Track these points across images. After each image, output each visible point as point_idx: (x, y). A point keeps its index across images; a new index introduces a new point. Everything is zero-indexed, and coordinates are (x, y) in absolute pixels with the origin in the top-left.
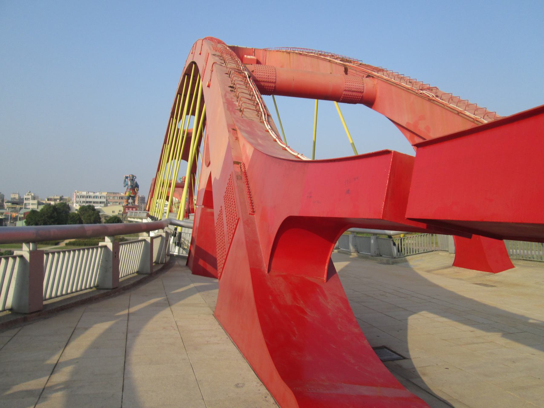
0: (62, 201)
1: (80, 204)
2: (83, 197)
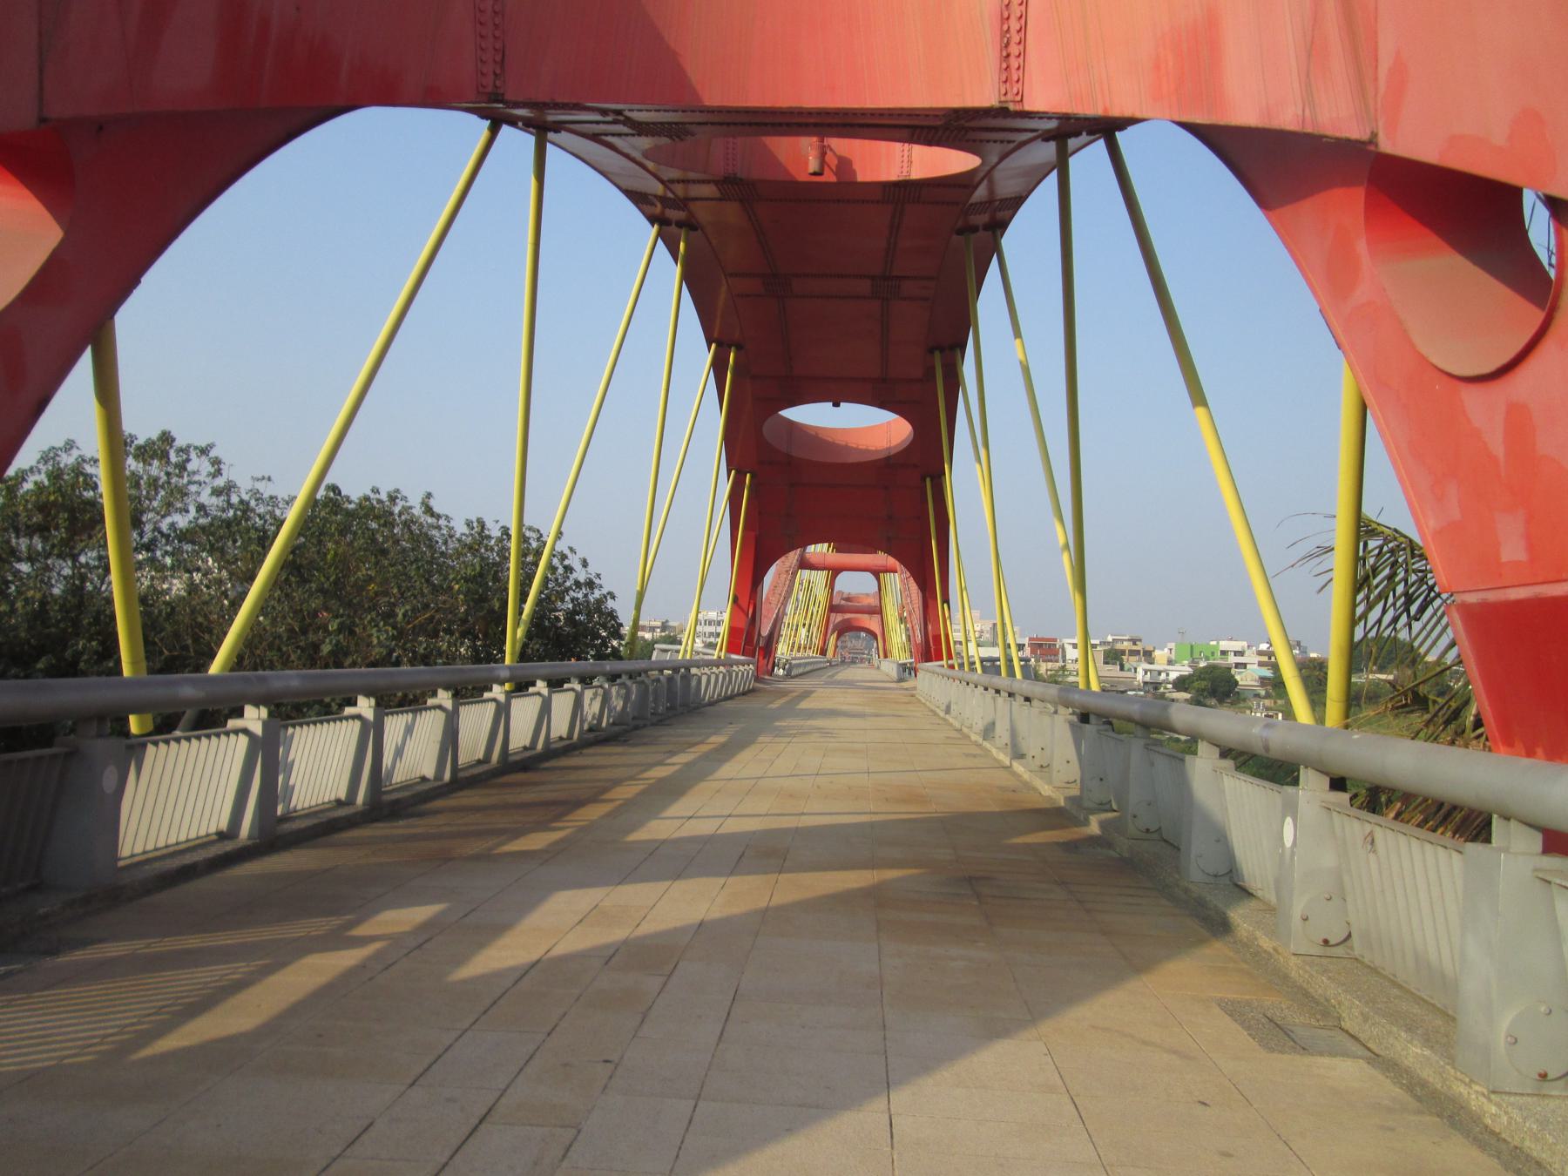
0: (667, 633)
1: (705, 639)
2: (710, 624)
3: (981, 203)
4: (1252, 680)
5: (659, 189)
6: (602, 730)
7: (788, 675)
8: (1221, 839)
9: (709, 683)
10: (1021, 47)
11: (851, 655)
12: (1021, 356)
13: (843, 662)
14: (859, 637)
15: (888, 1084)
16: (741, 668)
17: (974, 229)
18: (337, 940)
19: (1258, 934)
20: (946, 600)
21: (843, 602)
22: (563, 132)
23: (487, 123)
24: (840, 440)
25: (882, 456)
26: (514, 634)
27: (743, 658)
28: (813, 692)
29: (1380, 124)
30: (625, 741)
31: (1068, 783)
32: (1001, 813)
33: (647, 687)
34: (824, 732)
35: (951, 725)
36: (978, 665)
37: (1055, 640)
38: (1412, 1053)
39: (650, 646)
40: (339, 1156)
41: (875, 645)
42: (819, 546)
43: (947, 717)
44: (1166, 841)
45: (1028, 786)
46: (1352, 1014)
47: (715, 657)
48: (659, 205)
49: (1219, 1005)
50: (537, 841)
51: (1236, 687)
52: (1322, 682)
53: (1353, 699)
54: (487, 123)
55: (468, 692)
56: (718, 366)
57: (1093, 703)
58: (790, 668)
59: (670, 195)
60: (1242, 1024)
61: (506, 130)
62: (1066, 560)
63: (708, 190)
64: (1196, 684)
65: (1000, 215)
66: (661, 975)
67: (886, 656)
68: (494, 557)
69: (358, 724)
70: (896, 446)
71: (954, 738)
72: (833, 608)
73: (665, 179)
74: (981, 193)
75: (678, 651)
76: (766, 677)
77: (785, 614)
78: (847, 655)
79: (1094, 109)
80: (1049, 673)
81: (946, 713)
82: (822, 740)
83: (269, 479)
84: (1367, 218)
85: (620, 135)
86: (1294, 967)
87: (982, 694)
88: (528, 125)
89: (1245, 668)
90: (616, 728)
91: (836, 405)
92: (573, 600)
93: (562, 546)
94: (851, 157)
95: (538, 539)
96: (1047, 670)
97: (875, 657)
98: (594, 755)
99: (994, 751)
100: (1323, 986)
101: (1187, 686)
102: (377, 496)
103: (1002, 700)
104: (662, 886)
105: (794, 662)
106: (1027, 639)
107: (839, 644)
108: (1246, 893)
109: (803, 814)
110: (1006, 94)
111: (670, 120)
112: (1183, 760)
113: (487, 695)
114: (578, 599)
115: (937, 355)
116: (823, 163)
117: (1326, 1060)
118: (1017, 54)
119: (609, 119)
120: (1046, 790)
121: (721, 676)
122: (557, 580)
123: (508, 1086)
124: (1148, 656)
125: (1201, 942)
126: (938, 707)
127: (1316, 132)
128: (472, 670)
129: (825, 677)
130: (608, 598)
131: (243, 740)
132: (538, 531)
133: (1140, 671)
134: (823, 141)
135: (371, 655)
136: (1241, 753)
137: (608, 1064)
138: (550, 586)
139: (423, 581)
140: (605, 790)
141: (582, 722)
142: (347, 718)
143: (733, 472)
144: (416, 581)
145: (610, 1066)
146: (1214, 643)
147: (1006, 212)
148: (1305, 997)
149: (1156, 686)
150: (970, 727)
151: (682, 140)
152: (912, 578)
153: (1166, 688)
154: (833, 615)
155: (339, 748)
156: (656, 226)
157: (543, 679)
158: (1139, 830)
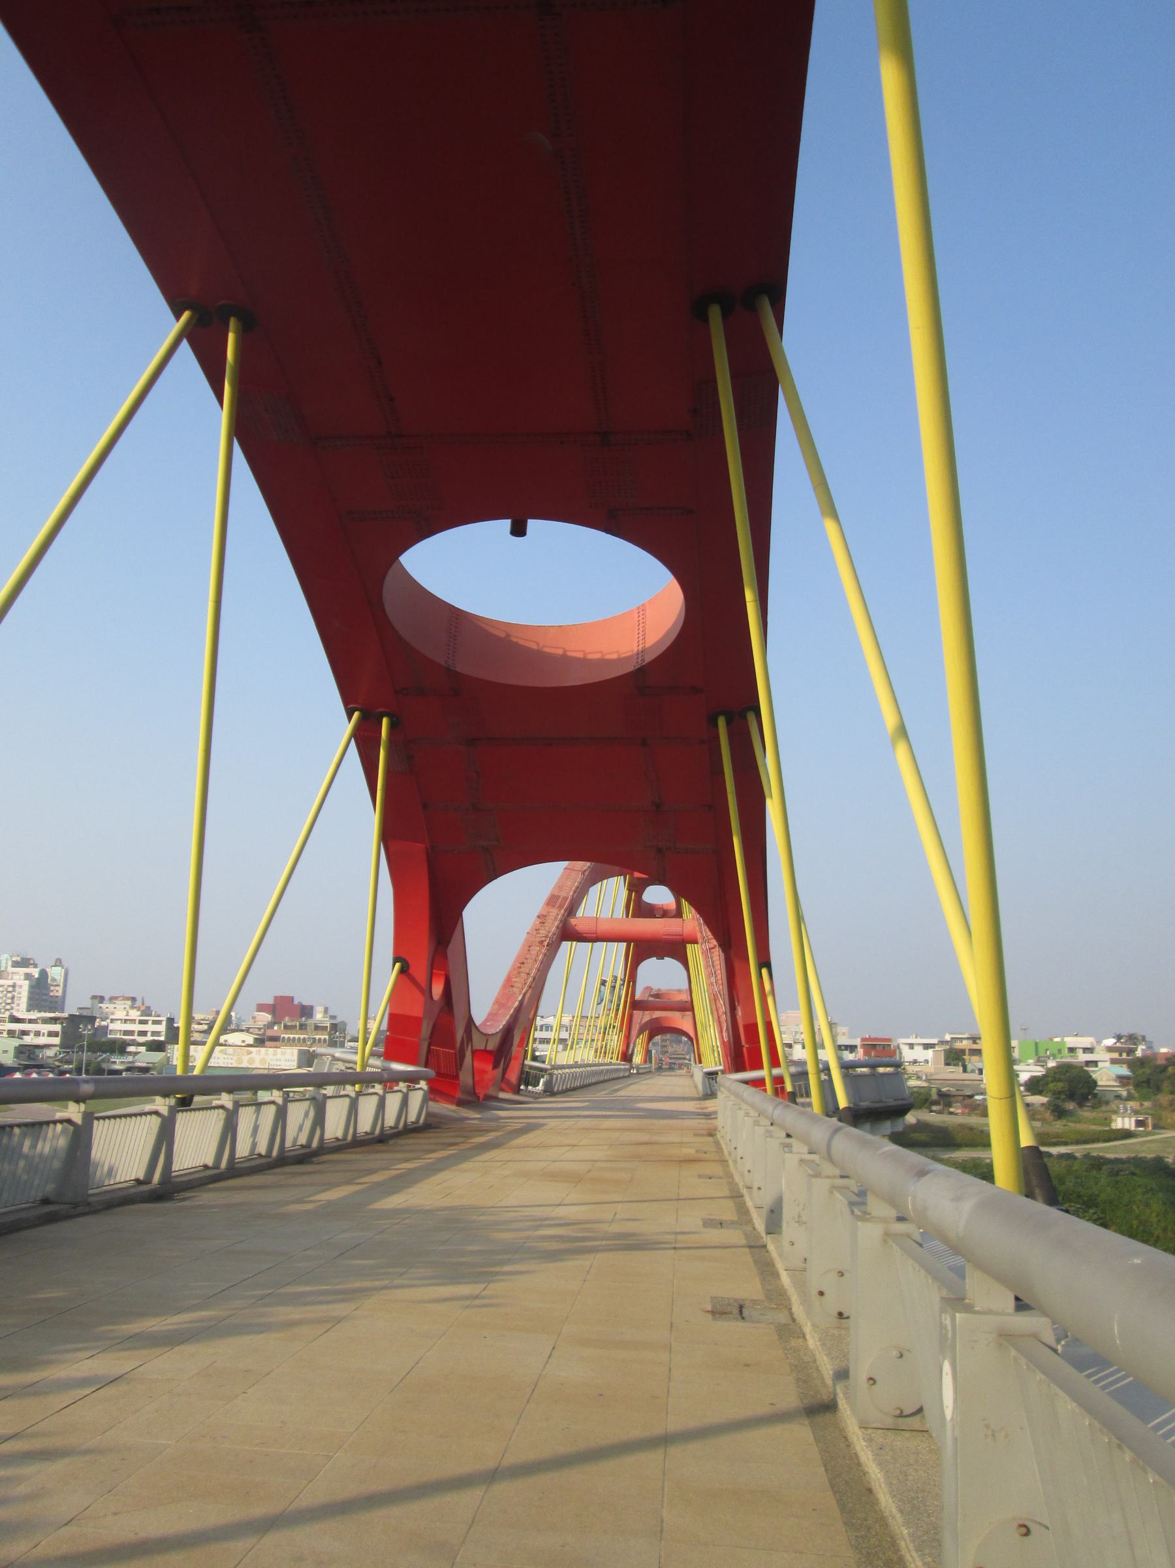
4: (1107, 1080)
14: (680, 1042)
20: (765, 962)
24: (553, 647)
25: (630, 668)
89: (1097, 1066)
101: (1041, 1088)
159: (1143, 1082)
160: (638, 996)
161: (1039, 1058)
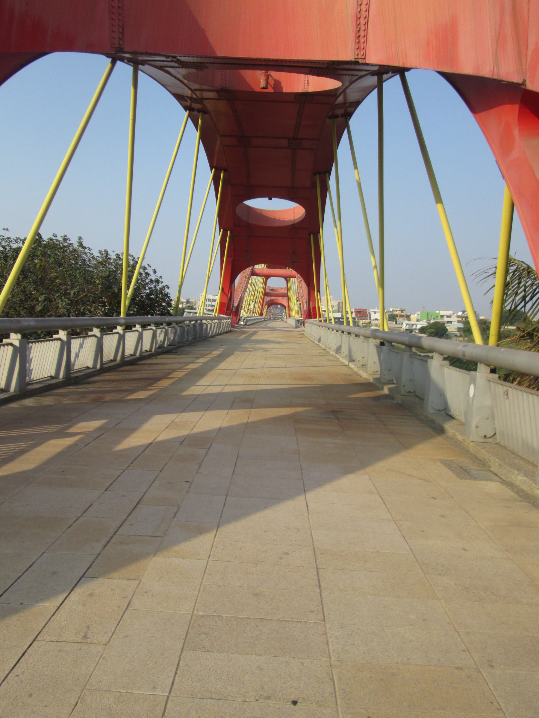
1: (206, 308)
2: (209, 301)
3: (341, 104)
4: (454, 329)
5: (188, 93)
6: (165, 348)
7: (246, 325)
8: (442, 395)
9: (211, 327)
10: (366, 32)
11: (273, 316)
12: (357, 178)
13: (270, 319)
14: (277, 308)
15: (305, 491)
16: (225, 321)
17: (337, 116)
18: (62, 434)
19: (457, 434)
20: (319, 291)
21: (270, 292)
22: (146, 65)
23: (110, 60)
25: (291, 223)
26: (124, 303)
27: (226, 316)
28: (258, 332)
29: (528, 76)
30: (175, 353)
31: (374, 372)
32: (345, 385)
33: (184, 329)
34: (264, 350)
35: (321, 347)
36: (333, 321)
37: (366, 310)
38: (519, 479)
39: (183, 310)
40: (81, 516)
41: (285, 311)
42: (260, 265)
43: (319, 344)
44: (417, 396)
45: (356, 373)
46: (495, 464)
47: (213, 316)
48: (189, 101)
49: (440, 462)
50: (143, 395)
51: (446, 332)
52: (488, 328)
53: (501, 336)
54: (110, 60)
55: (107, 329)
56: (216, 180)
57: (387, 336)
58: (246, 321)
59: (194, 96)
60: (449, 469)
61: (119, 63)
62: (375, 274)
63: (211, 95)
64: (429, 330)
65: (349, 110)
66: (206, 449)
67: (290, 316)
68: (113, 268)
69: (59, 342)
70: (298, 219)
71: (323, 353)
72: (266, 294)
73: (193, 88)
74: (340, 99)
75: (196, 313)
76: (236, 325)
77: (244, 297)
78: (272, 316)
79: (399, 63)
80: (363, 325)
81: (319, 342)
82: (264, 353)
83: (7, 230)
84: (519, 118)
85: (173, 67)
86: (471, 447)
87: (335, 333)
88: (129, 61)
90: (171, 347)
91: (270, 199)
92: (149, 288)
93: (145, 264)
94: (280, 81)
95: (133, 260)
96: (363, 324)
97: (284, 316)
98: (163, 358)
99: (341, 359)
100: (484, 454)
101: (425, 331)
102: (56, 238)
103: (345, 336)
104: (200, 413)
105: (248, 319)
106: (354, 309)
107: (268, 311)
108: (452, 417)
109: (258, 384)
110: (358, 55)
111: (198, 61)
112: (427, 361)
113: (114, 331)
114: (152, 288)
115: (318, 176)
116: (267, 82)
117: (483, 482)
118: (363, 36)
119: (169, 60)
120: (364, 375)
121: (216, 324)
122: (142, 279)
123: (147, 491)
124: (408, 317)
125: (432, 437)
126: (315, 339)
127: (498, 79)
128: (104, 319)
129: (262, 326)
130: (166, 287)
131: (11, 349)
132: (133, 256)
133: (404, 324)
134: (267, 73)
135: (59, 312)
136: (454, 358)
137: (187, 483)
138: (139, 282)
139: (82, 278)
140: (169, 374)
141: (156, 343)
142: (55, 340)
143: (222, 230)
144: (79, 279)
145: (189, 484)
146: (437, 312)
147: (352, 108)
148: (475, 458)
149: (411, 331)
150: (330, 348)
151: (202, 71)
152: (303, 281)
153: (415, 332)
154: (266, 297)
155: (51, 353)
156: (188, 112)
157: (139, 324)
158: (406, 392)
159: (467, 330)
160: (267, 291)
161: (428, 319)
